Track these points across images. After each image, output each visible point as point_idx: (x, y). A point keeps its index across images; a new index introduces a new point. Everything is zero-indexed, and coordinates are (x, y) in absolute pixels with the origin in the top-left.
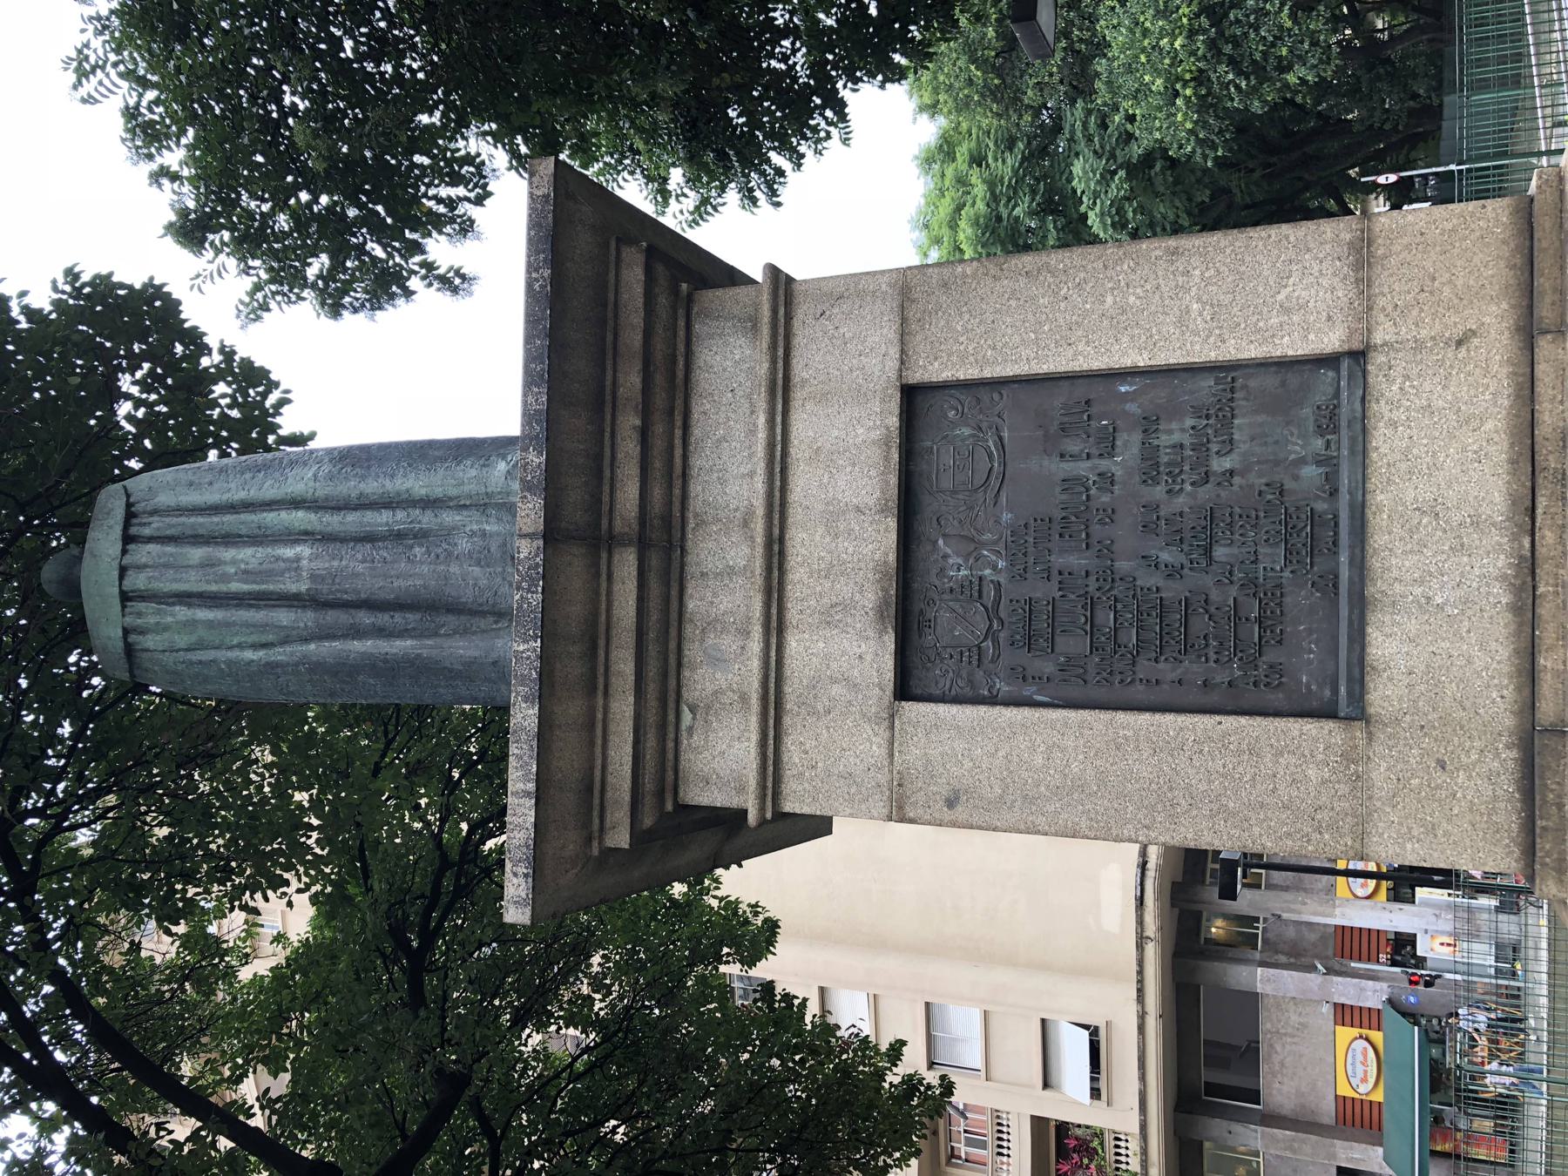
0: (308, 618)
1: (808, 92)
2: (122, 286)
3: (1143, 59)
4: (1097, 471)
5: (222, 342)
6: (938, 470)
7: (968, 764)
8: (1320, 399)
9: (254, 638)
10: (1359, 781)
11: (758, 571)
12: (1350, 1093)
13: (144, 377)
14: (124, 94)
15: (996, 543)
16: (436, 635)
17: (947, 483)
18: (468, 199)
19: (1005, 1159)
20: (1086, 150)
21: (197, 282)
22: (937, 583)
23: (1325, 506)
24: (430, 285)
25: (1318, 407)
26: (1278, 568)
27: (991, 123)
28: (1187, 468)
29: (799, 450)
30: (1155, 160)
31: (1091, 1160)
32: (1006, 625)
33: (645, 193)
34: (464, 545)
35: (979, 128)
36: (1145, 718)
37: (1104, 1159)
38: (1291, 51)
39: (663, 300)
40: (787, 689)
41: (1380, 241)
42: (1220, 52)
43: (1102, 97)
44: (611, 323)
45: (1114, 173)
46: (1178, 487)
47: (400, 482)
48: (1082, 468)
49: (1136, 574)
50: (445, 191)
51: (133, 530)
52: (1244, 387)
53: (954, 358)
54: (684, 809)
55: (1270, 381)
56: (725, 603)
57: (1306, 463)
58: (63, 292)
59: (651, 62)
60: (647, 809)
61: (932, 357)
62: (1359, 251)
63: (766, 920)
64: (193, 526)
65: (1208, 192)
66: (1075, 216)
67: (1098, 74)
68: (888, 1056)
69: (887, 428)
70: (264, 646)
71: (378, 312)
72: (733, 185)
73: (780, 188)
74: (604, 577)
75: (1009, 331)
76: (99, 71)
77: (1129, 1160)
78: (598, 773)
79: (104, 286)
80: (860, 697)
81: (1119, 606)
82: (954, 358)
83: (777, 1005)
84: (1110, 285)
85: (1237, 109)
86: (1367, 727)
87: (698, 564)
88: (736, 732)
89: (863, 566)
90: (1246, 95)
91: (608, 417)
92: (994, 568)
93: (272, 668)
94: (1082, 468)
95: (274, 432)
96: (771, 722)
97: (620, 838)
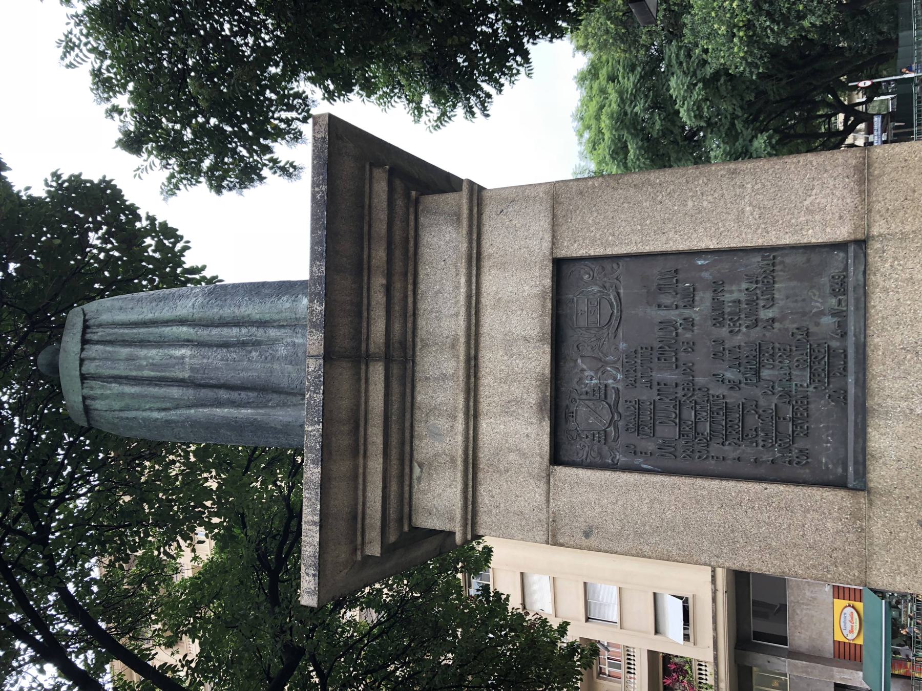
0: (190, 393)
1: (507, 45)
2: (87, 181)
3: (713, 14)
4: (683, 317)
5: (147, 213)
6: (577, 314)
7: (598, 510)
8: (834, 271)
9: (158, 405)
10: (863, 533)
11: (461, 378)
12: (843, 639)
13: (104, 234)
14: (92, 61)
15: (615, 362)
16: (266, 406)
17: (583, 322)
18: (298, 119)
19: (632, 676)
20: (678, 72)
21: (138, 172)
22: (577, 387)
23: (838, 344)
24: (275, 172)
25: (833, 277)
26: (805, 385)
27: (620, 56)
28: (743, 316)
29: (486, 300)
30: (721, 76)
31: (684, 677)
32: (623, 417)
33: (407, 109)
34: (282, 351)
35: (613, 59)
36: (715, 484)
37: (692, 677)
38: (805, 7)
39: (400, 203)
40: (481, 455)
41: (876, 165)
42: (761, 9)
43: (688, 38)
44: (367, 218)
45: (696, 85)
46: (737, 329)
47: (244, 310)
48: (673, 315)
49: (709, 386)
50: (284, 115)
51: (88, 336)
52: (782, 262)
53: (587, 241)
54: (414, 529)
55: (799, 259)
56: (440, 397)
57: (825, 315)
58: (51, 186)
59: (408, 32)
60: (392, 530)
61: (572, 240)
62: (862, 172)
63: (485, 548)
64: (122, 334)
65: (753, 95)
66: (672, 111)
67: (685, 25)
68: (558, 631)
69: (544, 287)
70: (164, 410)
71: (244, 190)
72: (460, 104)
73: (489, 105)
74: (363, 381)
75: (624, 224)
76: (76, 49)
77: (707, 678)
78: (360, 508)
79: (76, 182)
80: (528, 462)
81: (698, 407)
82: (587, 241)
83: (491, 599)
84: (691, 194)
85: (772, 43)
86: (868, 496)
87: (423, 372)
88: (448, 482)
89: (529, 376)
90: (777, 34)
91: (365, 278)
92: (615, 379)
93: (169, 423)
94: (673, 315)
95: (180, 266)
96: (470, 477)
97: (375, 550)
